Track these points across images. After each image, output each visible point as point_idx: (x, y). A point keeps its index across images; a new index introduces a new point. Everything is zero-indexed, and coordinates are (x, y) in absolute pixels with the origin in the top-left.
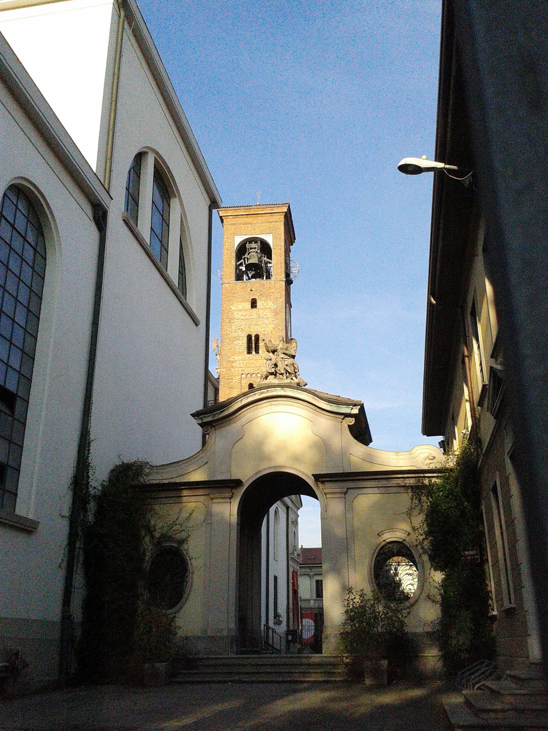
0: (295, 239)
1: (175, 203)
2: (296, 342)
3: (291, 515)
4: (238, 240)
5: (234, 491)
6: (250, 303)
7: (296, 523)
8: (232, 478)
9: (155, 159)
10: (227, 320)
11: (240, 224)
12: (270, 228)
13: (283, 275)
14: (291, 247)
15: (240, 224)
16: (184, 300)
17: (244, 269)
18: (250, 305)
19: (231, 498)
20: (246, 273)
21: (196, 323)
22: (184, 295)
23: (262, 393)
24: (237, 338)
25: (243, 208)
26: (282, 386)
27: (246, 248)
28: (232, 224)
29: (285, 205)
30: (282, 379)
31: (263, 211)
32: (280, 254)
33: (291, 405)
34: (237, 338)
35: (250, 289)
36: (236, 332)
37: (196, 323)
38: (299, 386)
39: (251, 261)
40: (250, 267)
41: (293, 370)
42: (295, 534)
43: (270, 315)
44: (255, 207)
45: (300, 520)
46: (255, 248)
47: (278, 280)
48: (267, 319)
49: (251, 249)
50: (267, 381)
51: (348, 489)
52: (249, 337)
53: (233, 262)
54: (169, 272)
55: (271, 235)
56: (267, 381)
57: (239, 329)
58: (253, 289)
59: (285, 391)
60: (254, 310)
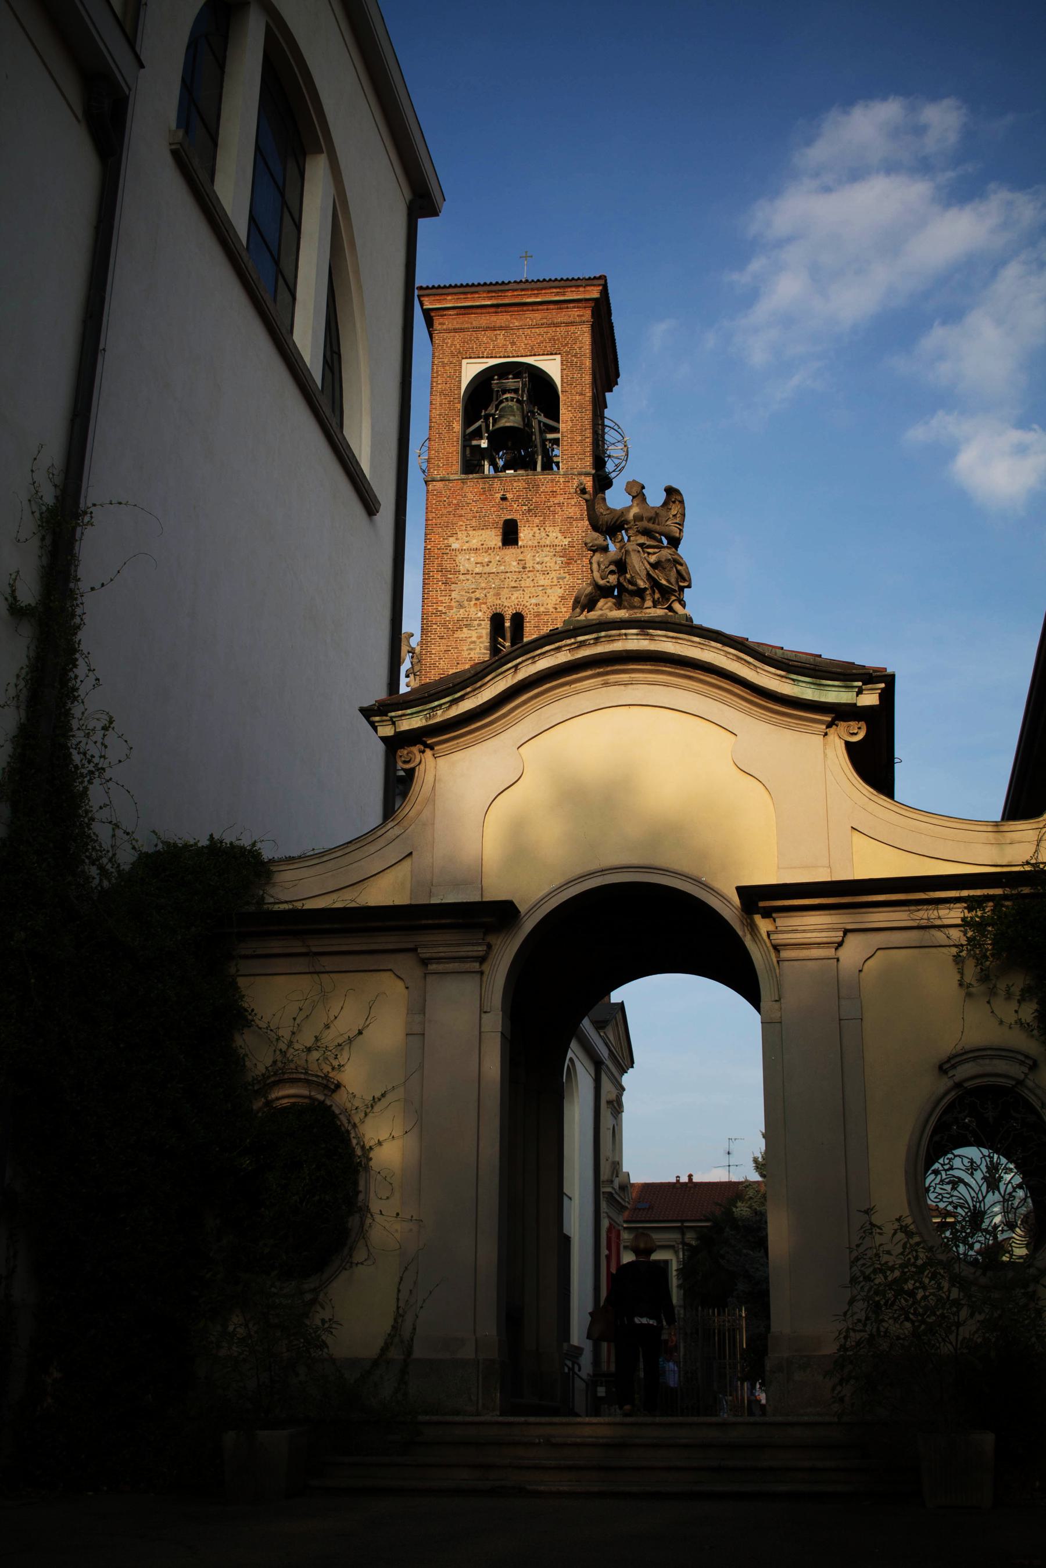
0: (618, 375)
1: (317, 171)
2: (682, 502)
3: (606, 1085)
4: (470, 370)
5: (491, 939)
6: (500, 532)
7: (617, 1107)
8: (487, 898)
9: (268, 26)
10: (438, 576)
11: (477, 329)
12: (553, 339)
13: (589, 461)
14: (607, 394)
15: (477, 329)
16: (337, 431)
17: (484, 444)
18: (500, 538)
19: (482, 960)
20: (489, 453)
21: (370, 506)
22: (338, 413)
23: (582, 644)
24: (465, 623)
25: (486, 288)
26: (644, 626)
27: (492, 390)
28: (455, 330)
29: (596, 282)
30: (641, 607)
31: (536, 295)
32: (581, 407)
33: (666, 685)
34: (465, 623)
35: (499, 496)
36: (461, 606)
37: (370, 506)
38: (688, 628)
39: (504, 423)
40: (501, 438)
41: (673, 580)
42: (616, 1133)
43: (553, 563)
44: (516, 286)
45: (625, 1098)
46: (516, 391)
47: (575, 472)
48: (545, 573)
49: (505, 392)
50: (594, 615)
51: (846, 932)
52: (497, 620)
53: (457, 426)
54: (297, 337)
55: (558, 357)
56: (594, 615)
57: (470, 600)
58: (509, 496)
59: (652, 638)
60: (511, 552)
